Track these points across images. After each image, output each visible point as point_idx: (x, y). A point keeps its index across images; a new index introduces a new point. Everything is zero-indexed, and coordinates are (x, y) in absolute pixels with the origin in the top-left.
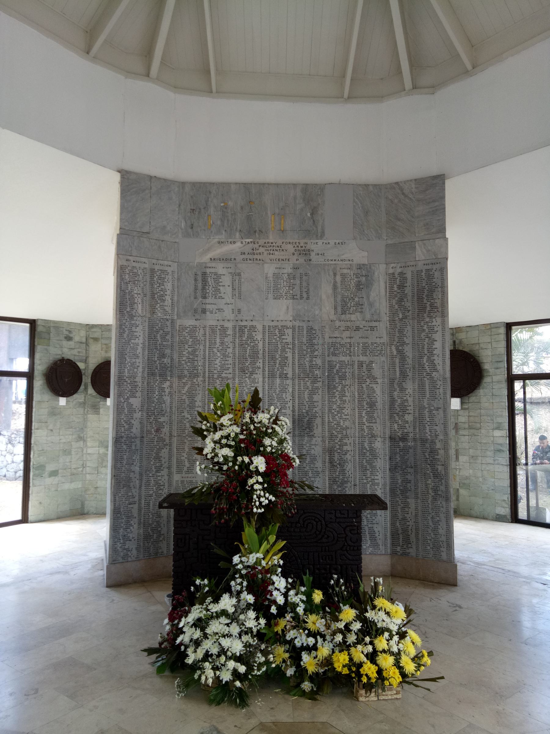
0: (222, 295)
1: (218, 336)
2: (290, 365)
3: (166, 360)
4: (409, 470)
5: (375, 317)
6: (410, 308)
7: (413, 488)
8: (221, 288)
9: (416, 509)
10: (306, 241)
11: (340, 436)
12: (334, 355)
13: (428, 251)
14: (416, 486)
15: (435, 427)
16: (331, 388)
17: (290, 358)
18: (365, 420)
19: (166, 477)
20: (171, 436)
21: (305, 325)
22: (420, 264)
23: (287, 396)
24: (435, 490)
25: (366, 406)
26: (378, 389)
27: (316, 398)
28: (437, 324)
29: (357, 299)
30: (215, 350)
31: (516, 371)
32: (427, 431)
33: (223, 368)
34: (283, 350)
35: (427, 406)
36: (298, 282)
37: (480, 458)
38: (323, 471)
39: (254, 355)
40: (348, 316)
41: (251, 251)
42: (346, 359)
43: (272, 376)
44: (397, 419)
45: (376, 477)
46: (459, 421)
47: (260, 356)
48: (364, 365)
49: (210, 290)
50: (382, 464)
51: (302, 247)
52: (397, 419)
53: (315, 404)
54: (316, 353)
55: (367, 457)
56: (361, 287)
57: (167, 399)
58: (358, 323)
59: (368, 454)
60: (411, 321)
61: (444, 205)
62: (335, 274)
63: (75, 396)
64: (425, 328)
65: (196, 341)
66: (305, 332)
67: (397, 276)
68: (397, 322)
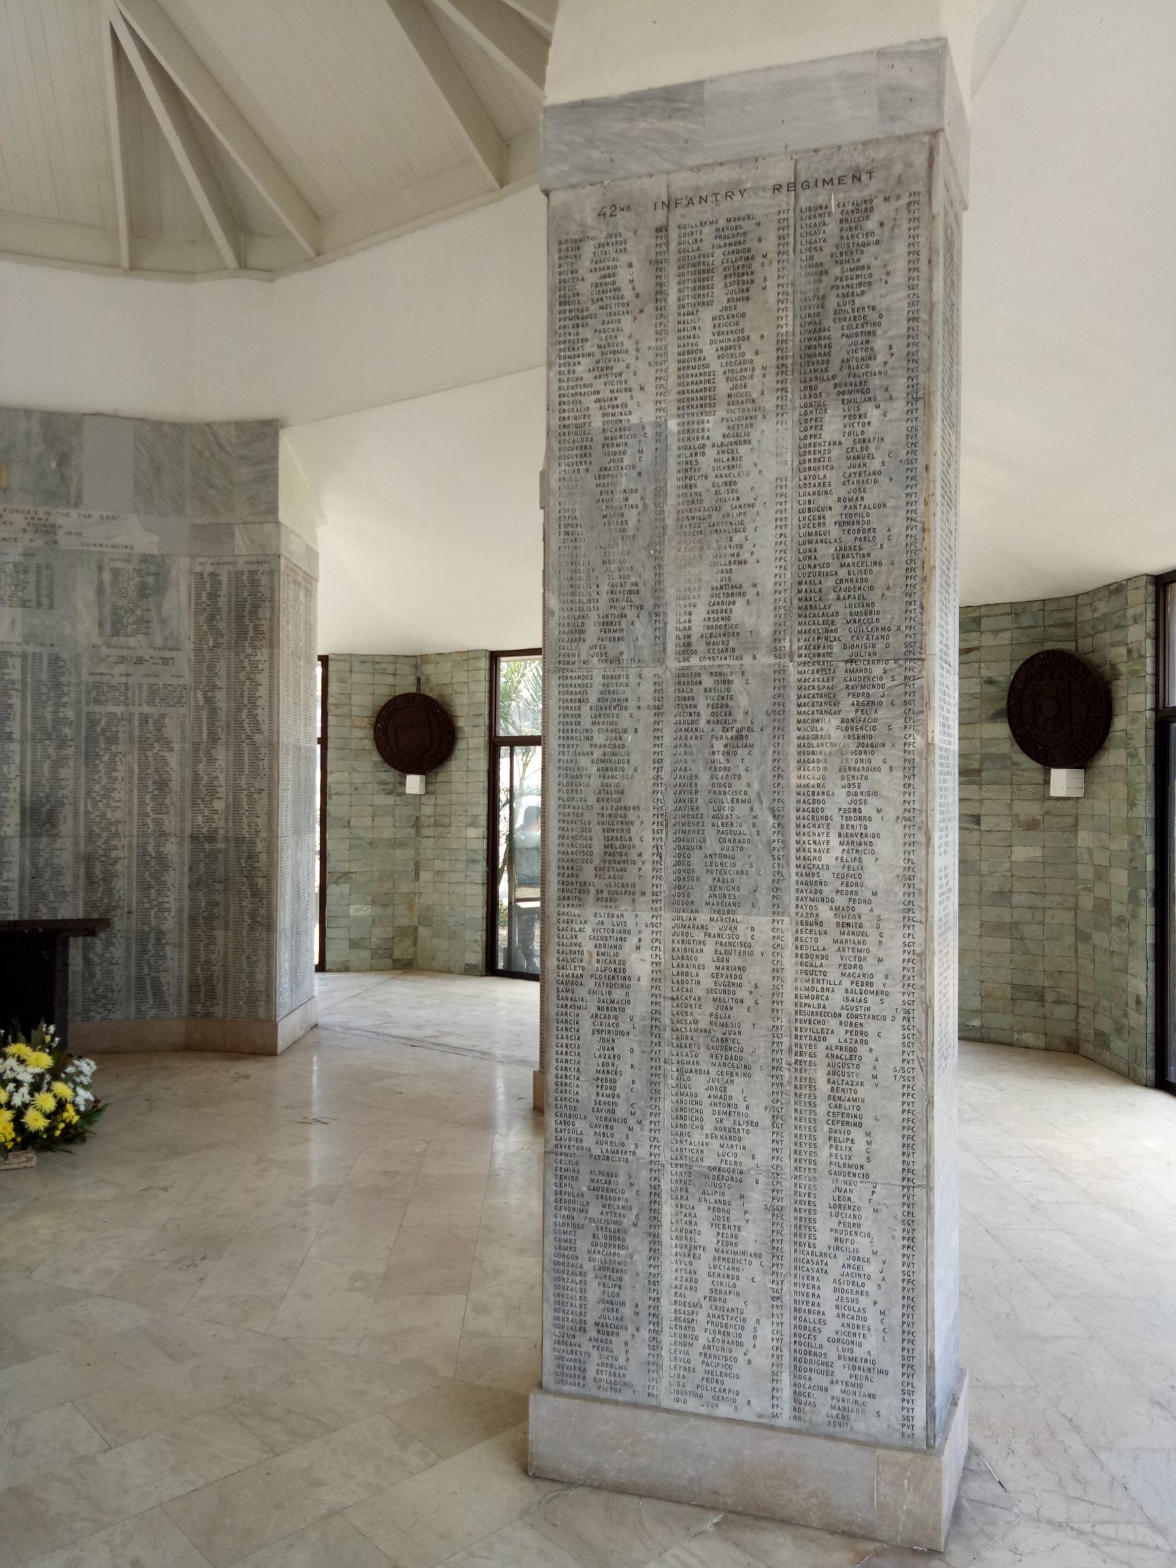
2: (18, 718)
4: (218, 886)
5: (171, 644)
6: (225, 632)
7: (222, 913)
9: (226, 945)
11: (105, 835)
12: (98, 702)
14: (227, 910)
15: (256, 820)
16: (90, 757)
18: (149, 809)
21: (45, 652)
22: (241, 560)
23: (11, 769)
24: (253, 915)
25: (151, 787)
26: (173, 760)
28: (263, 659)
29: (139, 612)
31: (505, 729)
32: (245, 825)
35: (245, 787)
36: (32, 578)
37: (447, 874)
38: (74, 892)
40: (123, 639)
42: (119, 710)
44: (202, 807)
45: (166, 899)
46: (422, 812)
48: (151, 721)
50: (176, 879)
51: (40, 519)
52: (202, 807)
53: (63, 783)
54: (65, 699)
55: (152, 868)
56: (147, 592)
58: (140, 652)
59: (153, 863)
60: (226, 653)
61: (277, 469)
62: (100, 569)
66: (45, 664)
67: (206, 577)
68: (205, 653)
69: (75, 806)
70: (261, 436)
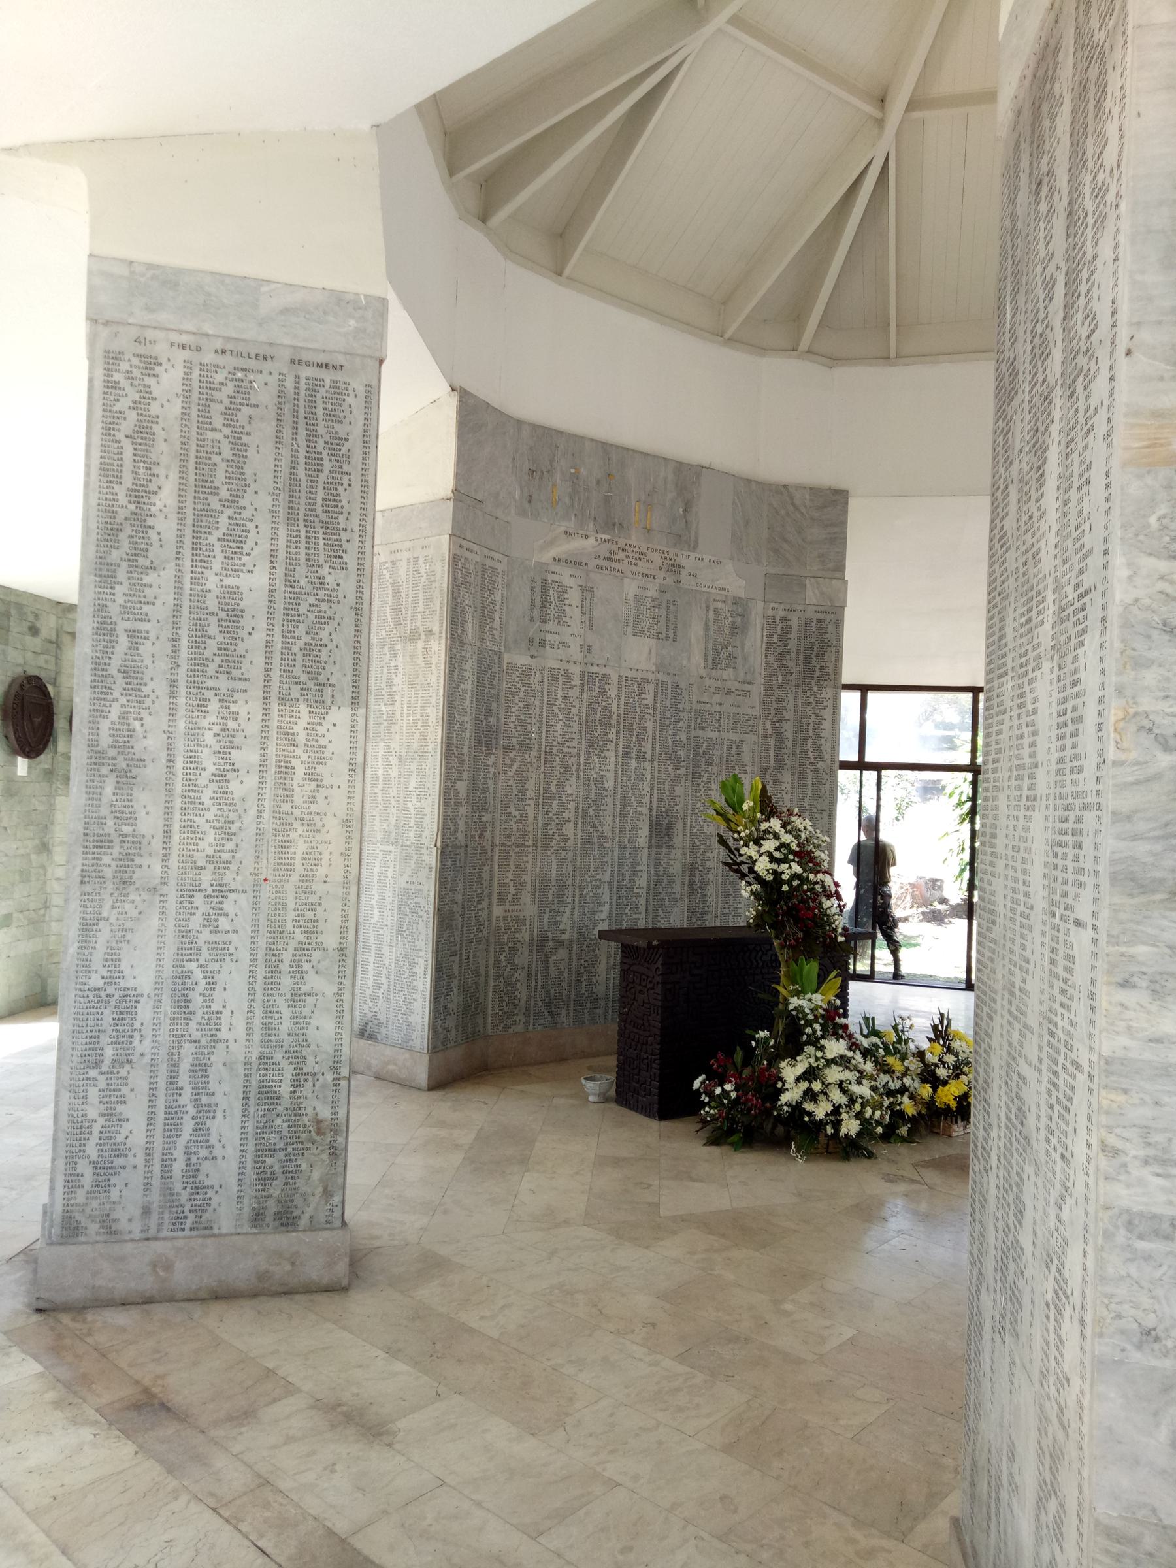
0: (567, 619)
1: (560, 686)
3: (492, 720)
5: (749, 678)
8: (567, 608)
10: (676, 551)
12: (702, 728)
13: (822, 593)
16: (695, 776)
17: (650, 730)
19: (486, 912)
20: (493, 845)
27: (679, 790)
28: (827, 696)
30: (555, 708)
33: (566, 738)
34: (642, 716)
36: (664, 613)
39: (606, 722)
41: (607, 555)
42: (714, 735)
43: (627, 755)
47: (614, 722)
49: (552, 609)
57: (490, 782)
58: (729, 684)
61: (846, 533)
63: (42, 757)
64: (811, 700)
65: (530, 693)
68: (775, 688)
69: (684, 820)
70: (831, 504)
